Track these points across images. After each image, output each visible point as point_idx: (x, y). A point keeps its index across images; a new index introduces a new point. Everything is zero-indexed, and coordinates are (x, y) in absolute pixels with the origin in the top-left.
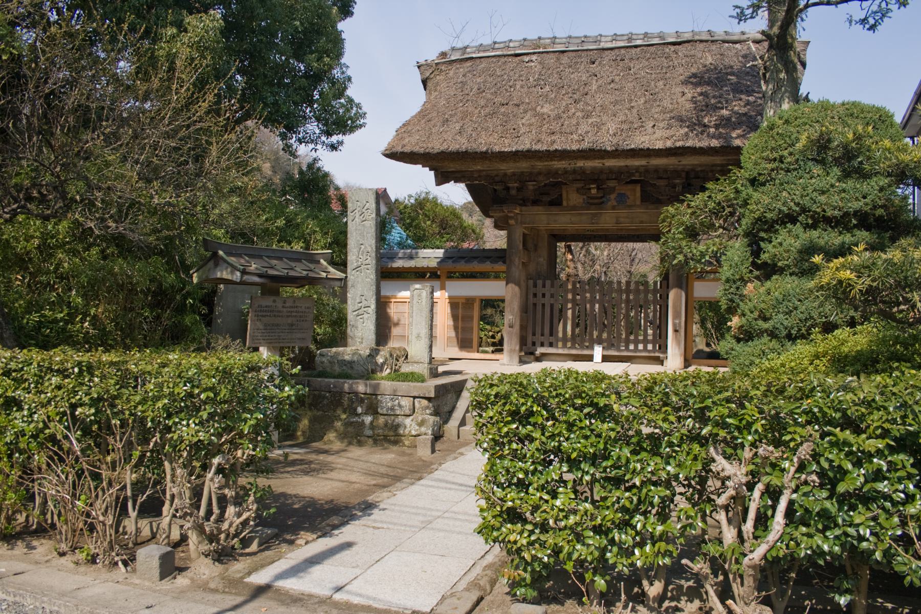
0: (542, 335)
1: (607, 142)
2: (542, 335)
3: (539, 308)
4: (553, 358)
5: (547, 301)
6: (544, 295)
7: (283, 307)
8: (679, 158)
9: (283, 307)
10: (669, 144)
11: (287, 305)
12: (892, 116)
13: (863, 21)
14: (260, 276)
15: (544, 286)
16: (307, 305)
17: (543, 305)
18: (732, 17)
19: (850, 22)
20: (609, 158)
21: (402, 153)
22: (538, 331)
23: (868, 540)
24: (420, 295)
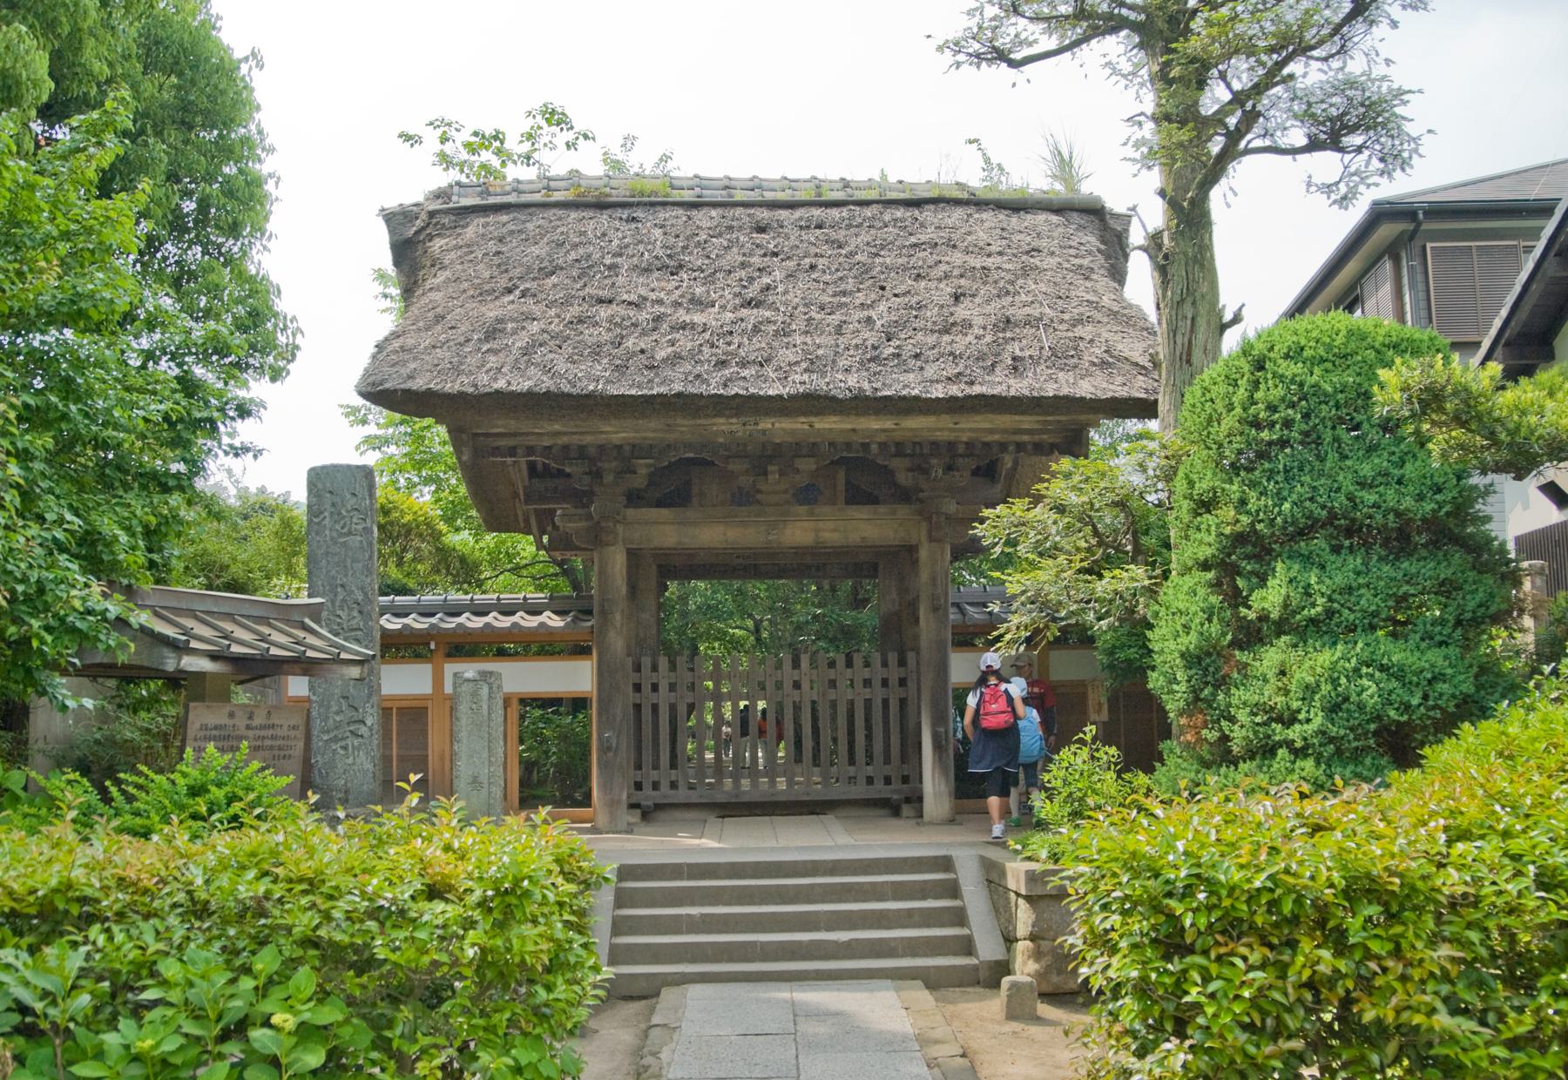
0: (656, 767)
1: (849, 381)
2: (656, 767)
3: (647, 713)
4: (677, 814)
5: (664, 697)
6: (655, 688)
7: (248, 727)
8: (957, 418)
9: (248, 727)
10: (955, 390)
11: (257, 722)
12: (276, 375)
13: (1328, 188)
14: (214, 657)
15: (655, 668)
16: (292, 723)
17: (655, 708)
18: (1134, 160)
19: (1309, 184)
20: (834, 412)
21: (408, 392)
22: (647, 758)
23: (1512, 1007)
24: (475, 694)
